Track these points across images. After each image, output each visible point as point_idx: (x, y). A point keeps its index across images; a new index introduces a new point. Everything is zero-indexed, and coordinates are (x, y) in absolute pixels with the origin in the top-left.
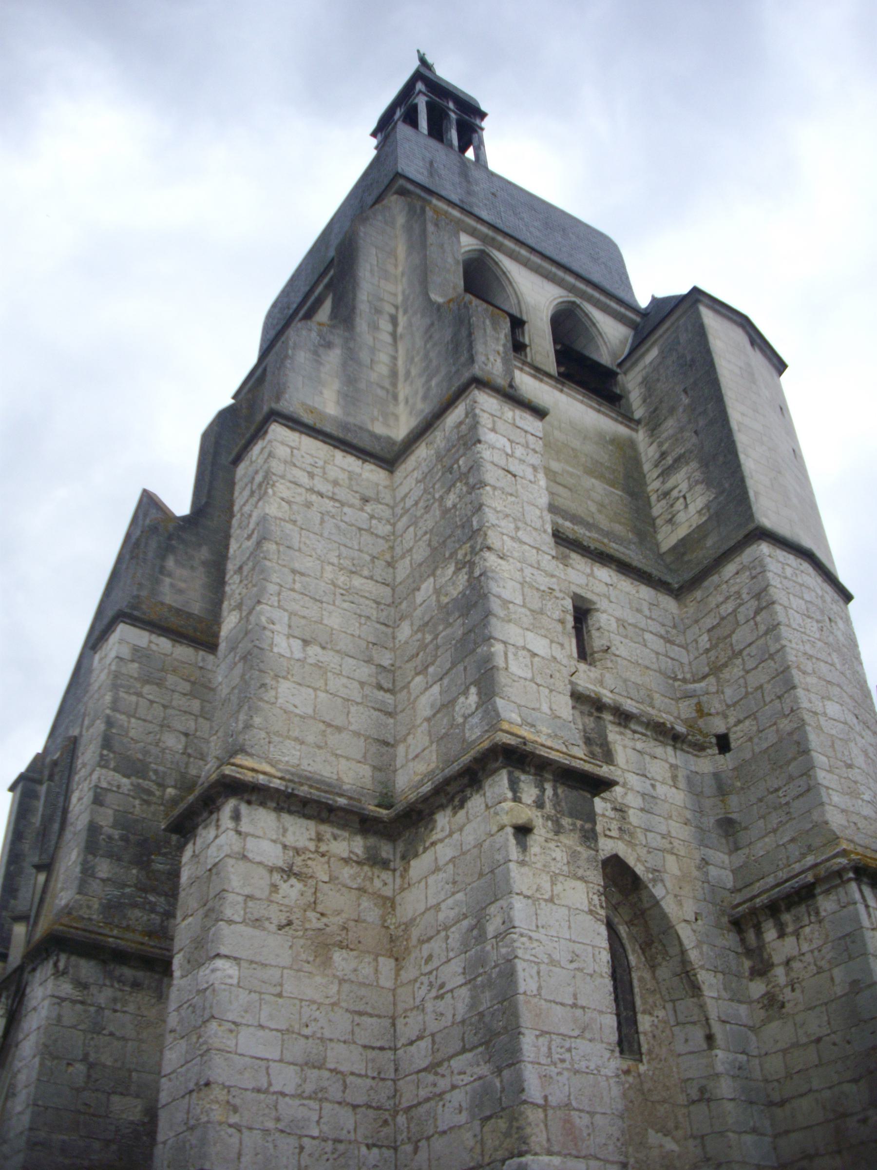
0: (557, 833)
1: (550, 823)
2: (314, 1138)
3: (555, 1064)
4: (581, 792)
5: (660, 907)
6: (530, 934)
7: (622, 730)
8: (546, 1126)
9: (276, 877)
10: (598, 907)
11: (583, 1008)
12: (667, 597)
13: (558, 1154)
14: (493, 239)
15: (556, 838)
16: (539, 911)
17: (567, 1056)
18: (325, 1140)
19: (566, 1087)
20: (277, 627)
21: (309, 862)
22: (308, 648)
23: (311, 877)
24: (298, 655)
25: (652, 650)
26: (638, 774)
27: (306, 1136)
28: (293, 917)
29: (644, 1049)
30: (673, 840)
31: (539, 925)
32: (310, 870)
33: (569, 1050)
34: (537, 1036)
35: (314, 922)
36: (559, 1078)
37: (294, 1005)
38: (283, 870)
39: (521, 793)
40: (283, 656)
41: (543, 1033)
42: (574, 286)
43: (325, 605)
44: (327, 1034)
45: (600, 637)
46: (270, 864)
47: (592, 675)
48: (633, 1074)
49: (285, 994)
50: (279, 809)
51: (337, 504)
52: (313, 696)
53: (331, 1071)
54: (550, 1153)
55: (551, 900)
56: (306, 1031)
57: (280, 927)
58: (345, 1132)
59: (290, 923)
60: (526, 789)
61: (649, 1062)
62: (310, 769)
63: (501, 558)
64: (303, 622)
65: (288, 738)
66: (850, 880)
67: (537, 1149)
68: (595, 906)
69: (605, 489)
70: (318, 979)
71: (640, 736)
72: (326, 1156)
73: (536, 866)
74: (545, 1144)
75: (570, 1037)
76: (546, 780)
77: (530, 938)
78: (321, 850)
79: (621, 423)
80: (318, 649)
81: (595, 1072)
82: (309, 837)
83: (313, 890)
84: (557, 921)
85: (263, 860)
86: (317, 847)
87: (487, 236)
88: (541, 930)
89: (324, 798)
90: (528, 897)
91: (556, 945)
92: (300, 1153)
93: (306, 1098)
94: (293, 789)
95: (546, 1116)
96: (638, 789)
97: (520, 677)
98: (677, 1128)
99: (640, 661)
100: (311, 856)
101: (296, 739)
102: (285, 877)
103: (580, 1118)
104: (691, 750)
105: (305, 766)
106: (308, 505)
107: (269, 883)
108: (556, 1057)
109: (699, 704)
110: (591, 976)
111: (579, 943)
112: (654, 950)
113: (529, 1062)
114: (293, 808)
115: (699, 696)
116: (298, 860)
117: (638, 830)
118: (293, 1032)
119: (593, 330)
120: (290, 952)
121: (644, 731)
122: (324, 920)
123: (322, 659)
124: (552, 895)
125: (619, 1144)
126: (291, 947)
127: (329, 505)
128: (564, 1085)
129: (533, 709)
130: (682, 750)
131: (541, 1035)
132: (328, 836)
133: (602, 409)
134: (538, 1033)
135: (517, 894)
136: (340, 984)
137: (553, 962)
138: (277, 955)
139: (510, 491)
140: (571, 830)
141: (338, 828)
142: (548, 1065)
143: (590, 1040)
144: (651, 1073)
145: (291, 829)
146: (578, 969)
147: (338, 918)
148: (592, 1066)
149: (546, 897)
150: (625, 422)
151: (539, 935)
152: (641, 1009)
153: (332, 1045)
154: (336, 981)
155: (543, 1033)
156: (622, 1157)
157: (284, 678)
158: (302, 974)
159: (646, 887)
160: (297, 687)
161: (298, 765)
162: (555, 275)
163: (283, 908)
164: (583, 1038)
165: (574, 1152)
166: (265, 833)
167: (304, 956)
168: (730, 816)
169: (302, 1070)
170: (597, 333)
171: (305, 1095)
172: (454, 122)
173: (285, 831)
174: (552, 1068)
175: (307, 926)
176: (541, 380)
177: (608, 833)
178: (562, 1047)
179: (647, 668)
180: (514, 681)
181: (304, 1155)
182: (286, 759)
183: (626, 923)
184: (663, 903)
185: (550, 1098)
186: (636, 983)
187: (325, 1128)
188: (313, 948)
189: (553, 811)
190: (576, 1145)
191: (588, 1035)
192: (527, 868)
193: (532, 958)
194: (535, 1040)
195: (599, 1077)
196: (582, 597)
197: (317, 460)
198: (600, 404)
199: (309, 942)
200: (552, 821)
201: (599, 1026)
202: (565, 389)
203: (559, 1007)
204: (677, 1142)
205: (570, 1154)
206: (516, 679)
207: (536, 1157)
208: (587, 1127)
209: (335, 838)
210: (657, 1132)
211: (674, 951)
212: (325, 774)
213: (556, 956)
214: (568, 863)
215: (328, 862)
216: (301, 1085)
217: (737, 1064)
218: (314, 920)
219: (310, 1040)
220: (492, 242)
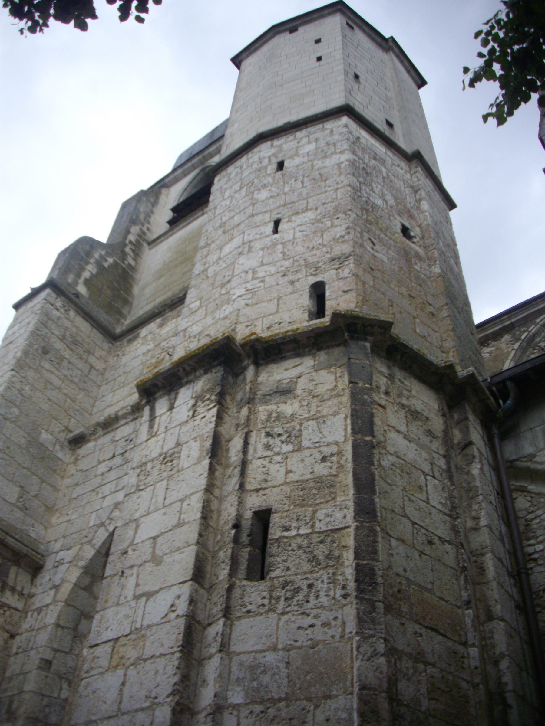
87: (200, 160)
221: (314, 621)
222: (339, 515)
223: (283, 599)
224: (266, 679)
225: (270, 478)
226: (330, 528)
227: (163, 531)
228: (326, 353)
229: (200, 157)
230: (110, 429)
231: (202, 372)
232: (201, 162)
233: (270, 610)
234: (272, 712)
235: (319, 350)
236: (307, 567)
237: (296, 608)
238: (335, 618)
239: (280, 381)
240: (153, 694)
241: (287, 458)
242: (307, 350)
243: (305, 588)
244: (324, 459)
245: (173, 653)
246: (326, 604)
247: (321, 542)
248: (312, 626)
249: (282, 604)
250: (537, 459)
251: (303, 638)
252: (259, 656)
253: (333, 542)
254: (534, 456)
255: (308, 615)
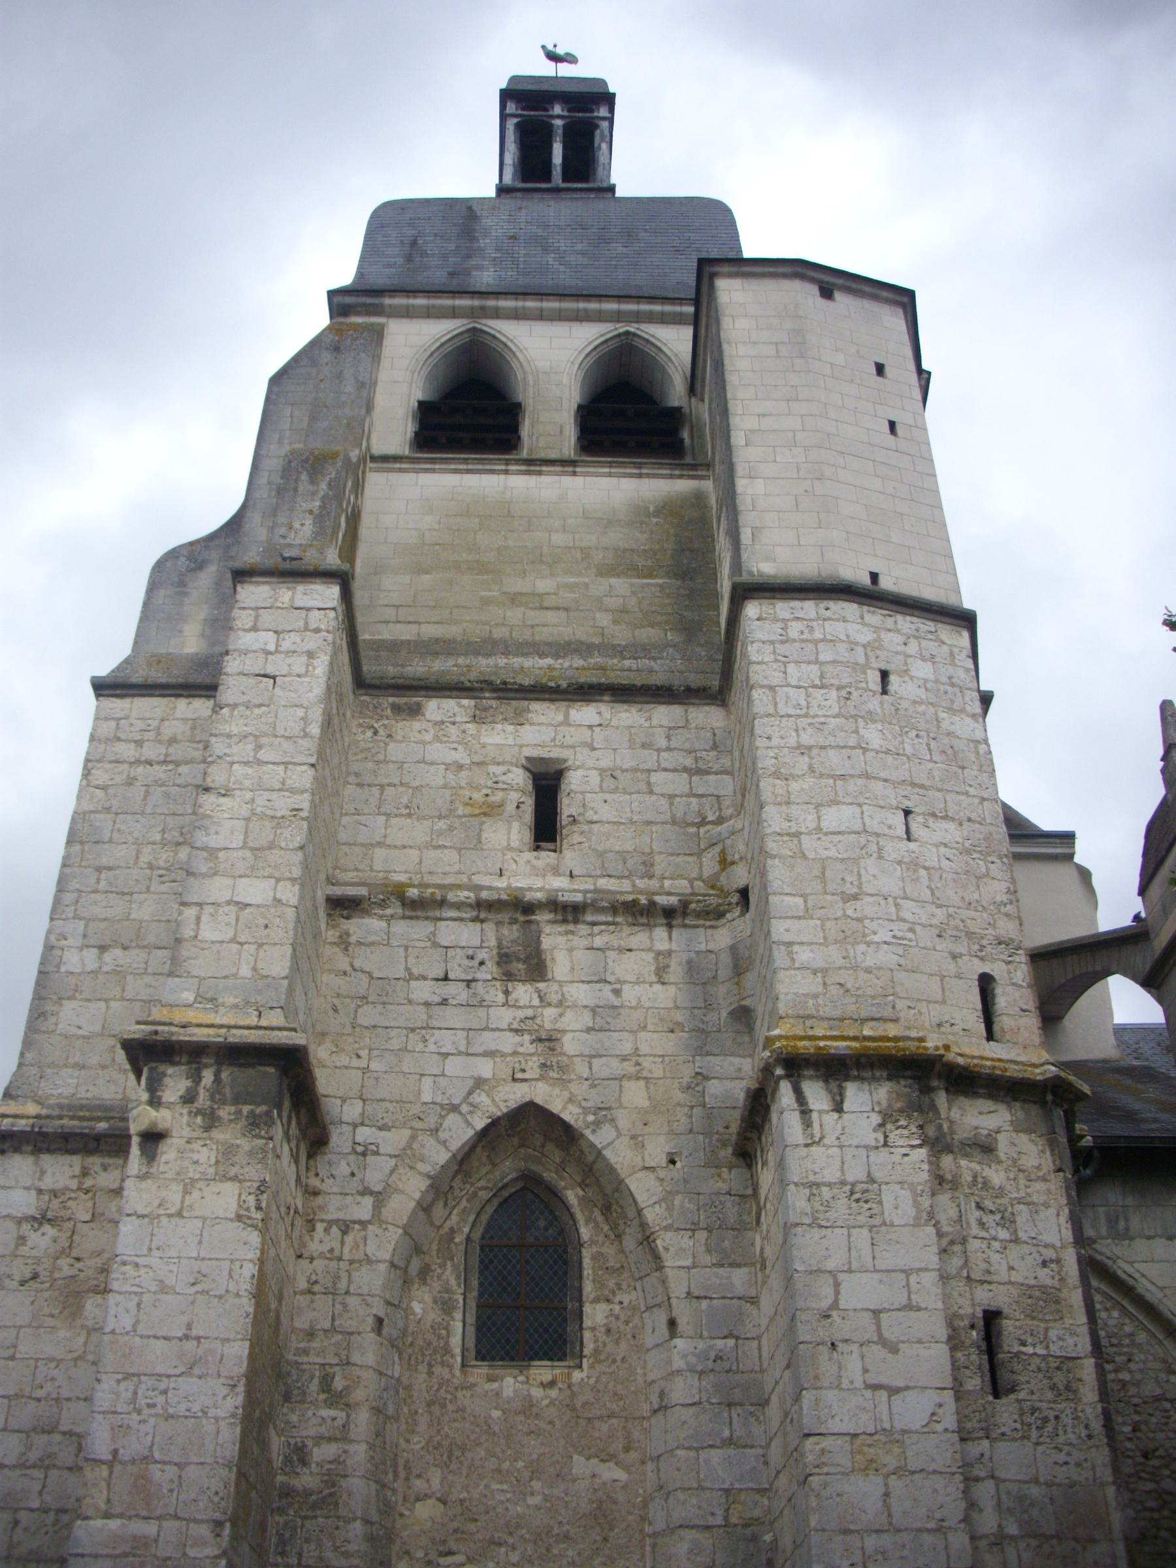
0: (207, 1129)
1: (199, 1119)
2: (32, 1510)
3: (139, 1412)
4: (262, 1069)
5: (605, 1159)
6: (137, 1260)
7: (571, 927)
8: (109, 1485)
9: (26, 1227)
10: (253, 1209)
11: (198, 1338)
12: (707, 708)
13: (120, 1516)
14: (483, 308)
15: (205, 1135)
16: (156, 1231)
17: (160, 1400)
18: (46, 1511)
19: (150, 1438)
20: (70, 942)
21: (70, 1203)
22: (106, 954)
23: (70, 1219)
24: (91, 965)
25: (662, 795)
26: (589, 982)
27: (24, 1509)
28: (40, 1269)
29: (586, 1352)
30: (641, 1060)
31: (154, 1246)
32: (70, 1211)
33: (165, 1392)
34: (118, 1381)
35: (65, 1267)
36: (142, 1427)
37: (28, 1366)
38: (34, 1219)
39: (163, 1091)
40: (72, 973)
41: (128, 1376)
42: (619, 312)
43: (135, 896)
44: (65, 1393)
45: (569, 805)
46: (19, 1215)
47: (540, 864)
48: (560, 1385)
49: (18, 1356)
50: (37, 1151)
51: (171, 767)
52: (104, 1009)
53: (64, 1433)
54: (107, 1516)
55: (179, 1214)
56: (40, 1393)
57: (22, 1283)
58: (72, 1500)
59: (35, 1277)
60: (171, 1084)
61: (592, 1367)
62: (89, 1095)
63: (224, 795)
64: (105, 924)
65: (66, 1066)
66: (780, 1078)
67: (90, 1512)
68: (248, 1209)
69: (632, 585)
70: (62, 1333)
71: (603, 927)
72: (45, 1529)
73: (166, 1176)
74: (103, 1506)
75: (169, 1376)
76: (206, 1066)
77: (137, 1265)
78: (85, 1186)
79: (681, 477)
80: (118, 952)
81: (200, 1414)
82: (71, 1174)
83: (69, 1233)
84: (182, 1237)
85: (11, 1211)
86: (80, 1183)
87: (472, 308)
88: (155, 1253)
89: (79, 1128)
90: (144, 1216)
91: (174, 1268)
92: (13, 1528)
93: (29, 1468)
94: (40, 1128)
95: (111, 1474)
96: (585, 1003)
97: (213, 942)
98: (627, 1449)
99: (635, 818)
100: (72, 1195)
101: (76, 1065)
102: (36, 1225)
103: (163, 1471)
104: (701, 922)
105: (82, 1094)
106: (130, 782)
107: (15, 1236)
108: (142, 1402)
109: (723, 852)
110: (220, 1297)
111: (210, 1259)
112: (614, 1215)
113: (99, 1413)
114: (53, 1147)
115: (723, 841)
116: (56, 1203)
117: (577, 1060)
118: (23, 1396)
119: (660, 358)
120: (31, 1308)
121: (610, 919)
122: (79, 1265)
123: (122, 963)
124: (182, 1208)
125: (216, 1499)
126: (32, 1303)
127: (159, 772)
128: (147, 1434)
129: (226, 977)
130: (685, 926)
131: (125, 1379)
132: (97, 1168)
133: (644, 471)
134: (120, 1376)
135: (128, 1215)
136: (89, 1334)
137: (164, 1288)
138: (15, 1314)
139: (260, 701)
140: (231, 1121)
141: (110, 1157)
142: (129, 1413)
143: (200, 1377)
144: (592, 1381)
145: (50, 1171)
146: (202, 1292)
147: (97, 1260)
148: (196, 1408)
149: (172, 1211)
150: (685, 473)
151: (153, 1261)
152: (592, 1296)
153: (69, 1404)
154: (85, 1332)
155: (128, 1376)
156: (218, 1514)
157: (69, 998)
158: (42, 1330)
159: (582, 1135)
160: (86, 1004)
161: (74, 1095)
162: (586, 310)
163: (29, 1261)
164: (191, 1375)
165: (144, 1513)
166: (17, 1182)
167: (46, 1311)
168: (743, 1003)
169: (28, 1436)
170: (665, 359)
171: (28, 1464)
172: (560, 132)
173: (43, 1172)
174: (135, 1416)
175: (57, 1275)
176: (540, 473)
177: (519, 1075)
178: (154, 1390)
179: (649, 823)
180: (203, 949)
181: (19, 1530)
182: (60, 1091)
183: (580, 1185)
184: (607, 1153)
185: (121, 1451)
186: (587, 1262)
187: (48, 1498)
188: (62, 1299)
189: (208, 1103)
190: (148, 1504)
191: (196, 1371)
192: (149, 1181)
193: (135, 1289)
194: (115, 1385)
195: (204, 1421)
196: (542, 759)
197: (150, 722)
198: (639, 466)
199: (57, 1293)
200: (204, 1115)
201: (219, 1357)
202: (578, 469)
203: (160, 1344)
204: (626, 1468)
205: (137, 1516)
206: (207, 946)
207: (86, 1522)
208: (172, 1481)
209: (105, 1168)
210: (588, 1459)
211: (631, 1213)
212: (106, 1096)
213: (170, 1281)
214: (217, 1162)
215: (93, 1198)
216: (24, 1454)
217: (713, 1355)
218: (66, 1268)
219: (43, 1402)
220: (484, 313)
221: (1068, 1459)
222: (1070, 1341)
223: (1034, 1427)
224: (1035, 1512)
225: (992, 1270)
226: (1064, 1354)
227: (886, 1306)
228: (1023, 1109)
229: (476, 303)
230: (419, 913)
231: (885, 1074)
232: (472, 313)
233: (1023, 1438)
234: (1046, 1547)
235: (1015, 1100)
236: (1050, 1395)
237: (1048, 1440)
238: (1086, 1460)
239: (976, 1128)
240: (938, 1515)
241: (1005, 1248)
242: (1002, 1094)
243: (1052, 1418)
244: (1044, 1264)
245: (953, 1474)
246: (1075, 1442)
247: (1058, 1368)
248: (1066, 1463)
249: (1034, 1434)
250: (1096, 1246)
251: (1061, 1475)
252: (1024, 1487)
253: (1069, 1371)
254: (1094, 1242)
255: (1061, 1451)
